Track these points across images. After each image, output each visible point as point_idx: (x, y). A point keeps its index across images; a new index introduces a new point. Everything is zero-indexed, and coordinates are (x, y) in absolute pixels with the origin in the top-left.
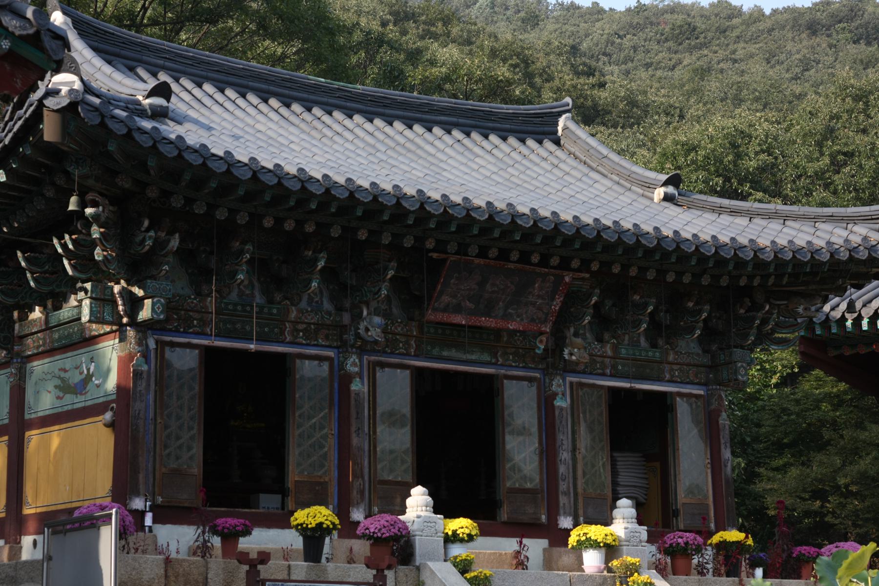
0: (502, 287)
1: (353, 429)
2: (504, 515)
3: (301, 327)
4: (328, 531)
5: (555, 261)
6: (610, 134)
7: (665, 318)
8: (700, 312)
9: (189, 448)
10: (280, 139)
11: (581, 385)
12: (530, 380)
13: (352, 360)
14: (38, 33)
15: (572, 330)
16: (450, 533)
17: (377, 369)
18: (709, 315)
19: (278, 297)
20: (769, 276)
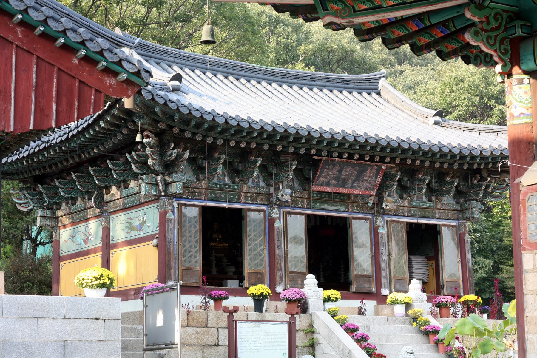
1: (276, 246)
2: (353, 288)
3: (249, 195)
4: (266, 297)
5: (377, 159)
6: (413, 70)
7: (435, 186)
8: (453, 182)
9: (195, 257)
10: (236, 99)
11: (392, 221)
12: (366, 219)
14: (139, 71)
15: (387, 193)
16: (326, 297)
17: (288, 215)
18: (458, 184)
19: (237, 180)
20: (489, 163)
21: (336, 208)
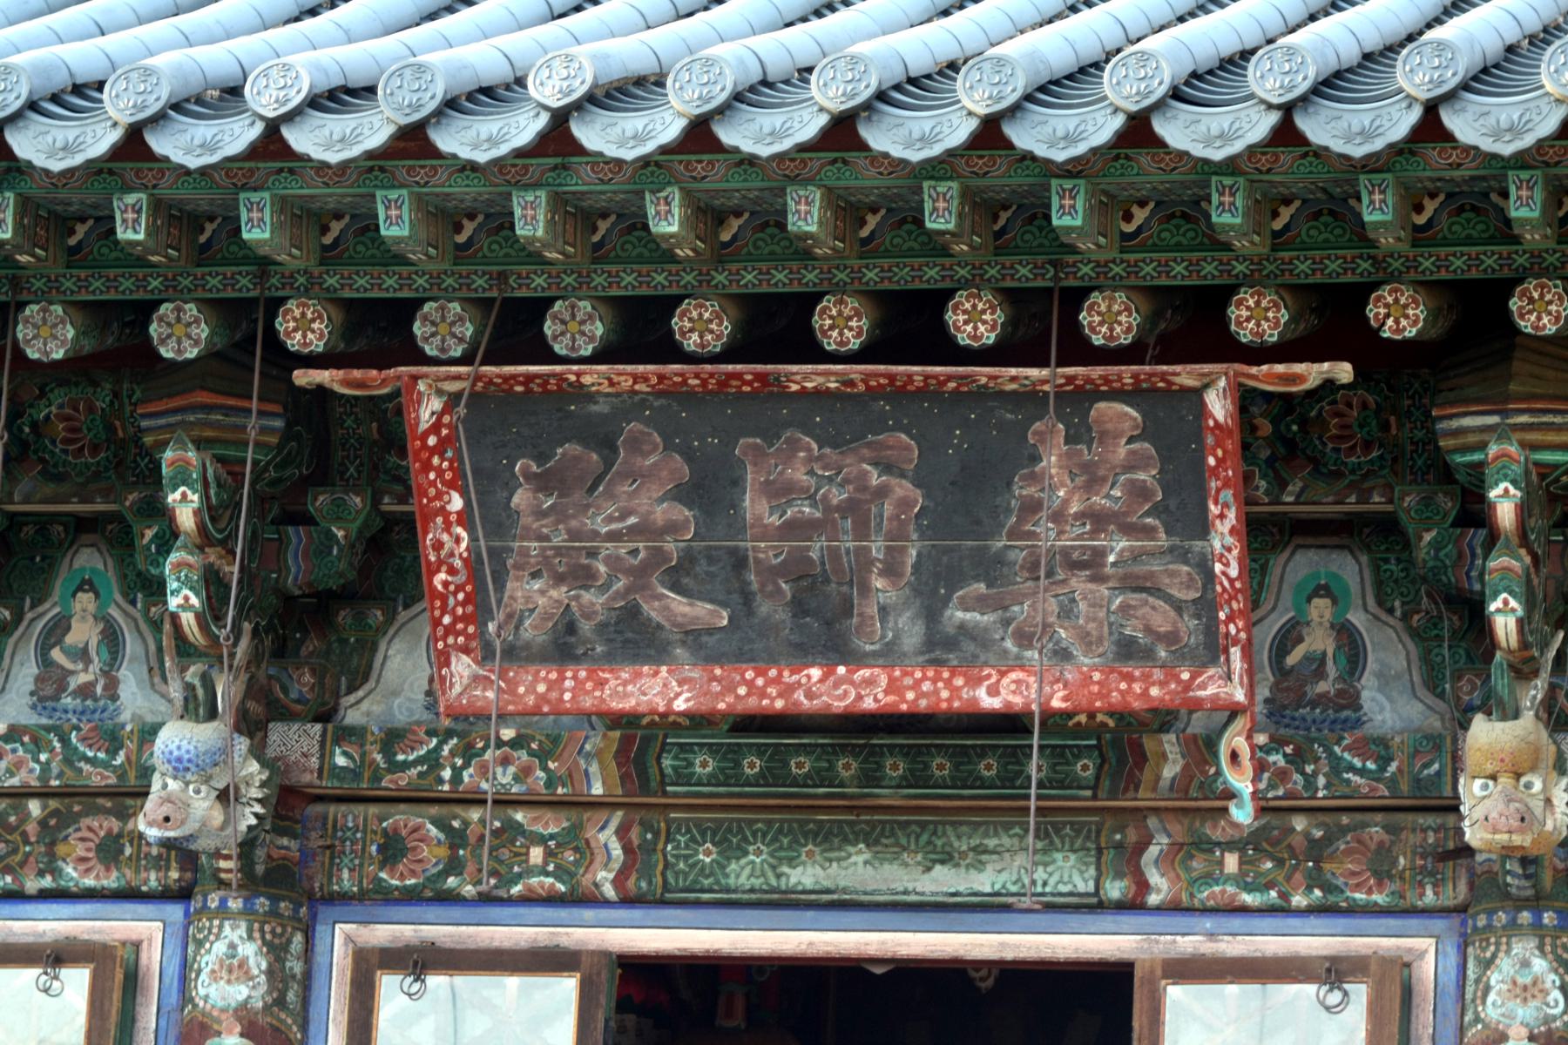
0: (838, 496)
12: (1334, 972)
13: (220, 948)
21: (985, 881)
